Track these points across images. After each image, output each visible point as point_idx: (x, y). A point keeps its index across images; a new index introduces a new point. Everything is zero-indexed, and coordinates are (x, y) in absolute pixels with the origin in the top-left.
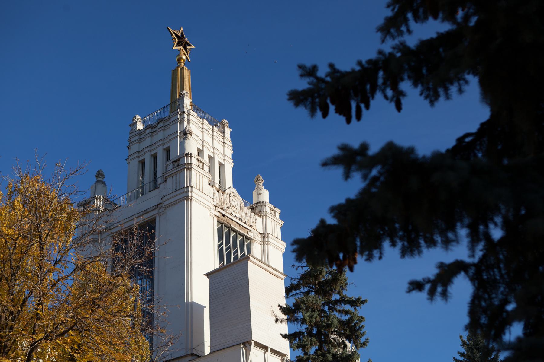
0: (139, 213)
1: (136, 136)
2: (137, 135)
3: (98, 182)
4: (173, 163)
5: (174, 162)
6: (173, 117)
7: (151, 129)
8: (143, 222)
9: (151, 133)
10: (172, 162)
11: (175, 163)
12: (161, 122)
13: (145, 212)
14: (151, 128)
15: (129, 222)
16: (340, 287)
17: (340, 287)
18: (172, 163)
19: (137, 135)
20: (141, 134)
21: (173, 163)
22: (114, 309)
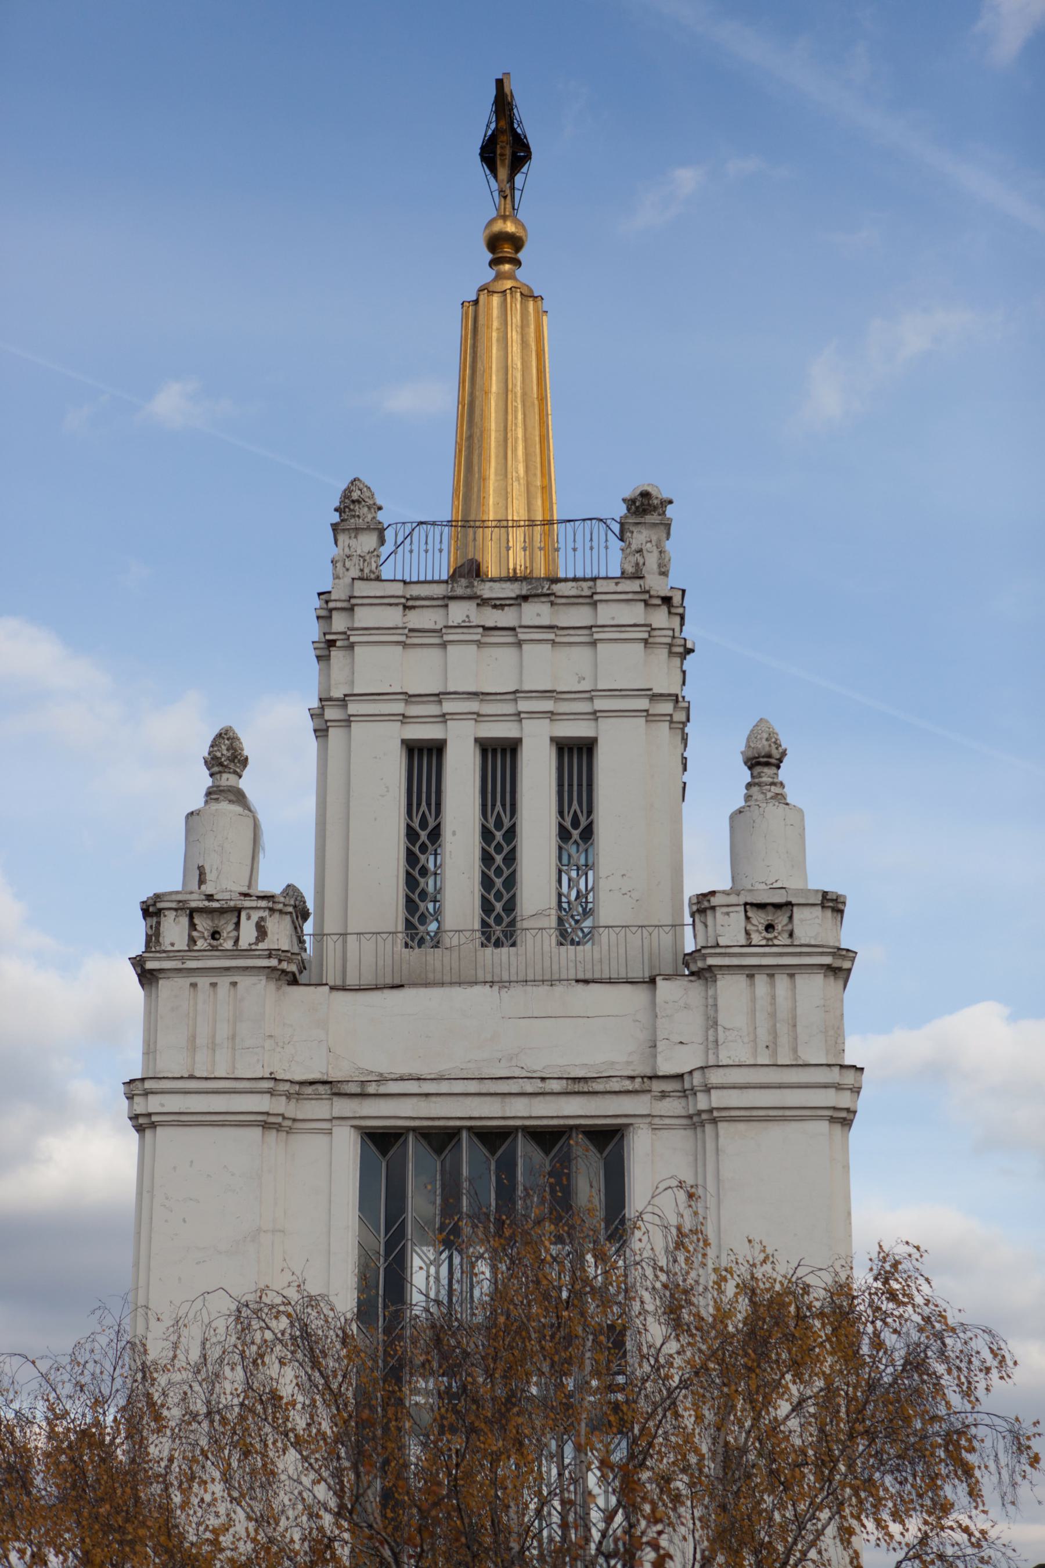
0: (543, 1079)
1: (137, 1264)
2: (397, 605)
3: (212, 794)
4: (746, 911)
5: (752, 905)
6: (313, 1102)
7: (478, 605)
8: (441, 1205)
9: (480, 630)
10: (746, 904)
11: (755, 909)
12: (543, 599)
13: (577, 1087)
14: (479, 601)
15: (477, 1100)
16: (331, 1540)
17: (331, 1540)
18: (742, 908)
19: (397, 605)
20: (410, 603)
21: (748, 907)
22: (768, 1285)
